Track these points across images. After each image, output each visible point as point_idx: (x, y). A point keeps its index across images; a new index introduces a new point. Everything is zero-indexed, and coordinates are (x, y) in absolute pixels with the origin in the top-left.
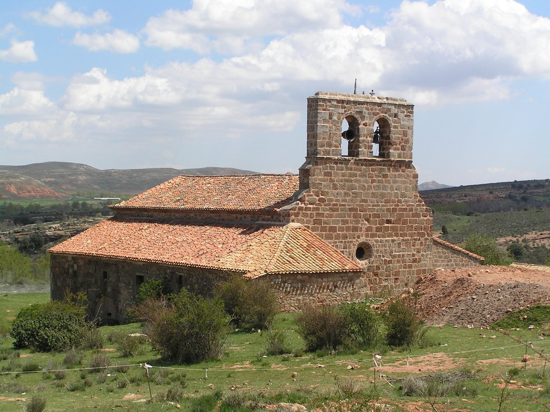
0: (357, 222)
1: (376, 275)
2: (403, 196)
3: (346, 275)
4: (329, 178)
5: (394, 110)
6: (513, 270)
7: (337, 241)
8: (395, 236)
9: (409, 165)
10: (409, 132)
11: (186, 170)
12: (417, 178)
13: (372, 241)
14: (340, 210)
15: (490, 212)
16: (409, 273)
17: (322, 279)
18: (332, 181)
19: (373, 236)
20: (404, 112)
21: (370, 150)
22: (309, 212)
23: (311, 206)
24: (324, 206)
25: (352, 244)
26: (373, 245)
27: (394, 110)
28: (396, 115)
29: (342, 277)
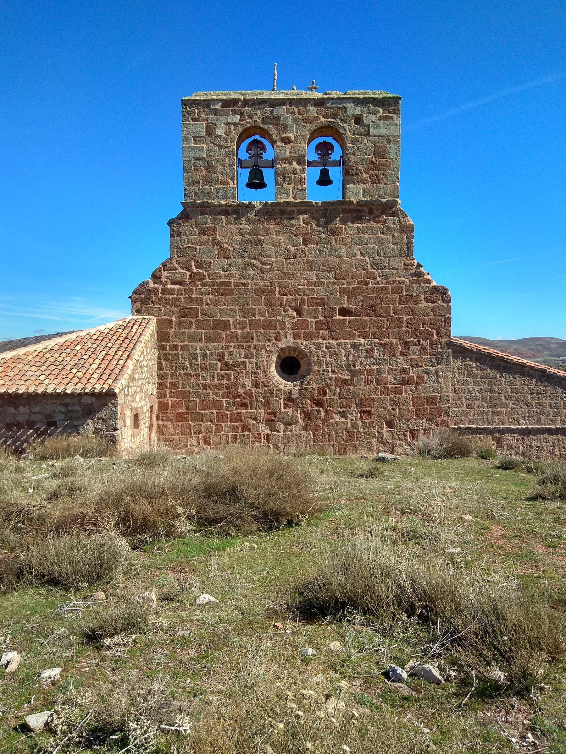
0: (275, 312)
1: (319, 404)
2: (377, 265)
3: (76, 400)
4: (211, 238)
5: (354, 110)
6: (194, 469)
7: (232, 345)
8: (359, 336)
9: (390, 208)
10: (392, 150)
11: (523, 342)
12: (413, 231)
13: (305, 345)
14: (235, 292)
15: (221, 100)
16: (395, 403)
17: (16, 408)
18: (216, 243)
19: (309, 336)
20: (376, 113)
21: (300, 187)
22: (171, 297)
23: (176, 287)
24: (202, 285)
25: (264, 350)
26: (310, 352)
27: (354, 110)
28: (358, 120)
29: (66, 405)
